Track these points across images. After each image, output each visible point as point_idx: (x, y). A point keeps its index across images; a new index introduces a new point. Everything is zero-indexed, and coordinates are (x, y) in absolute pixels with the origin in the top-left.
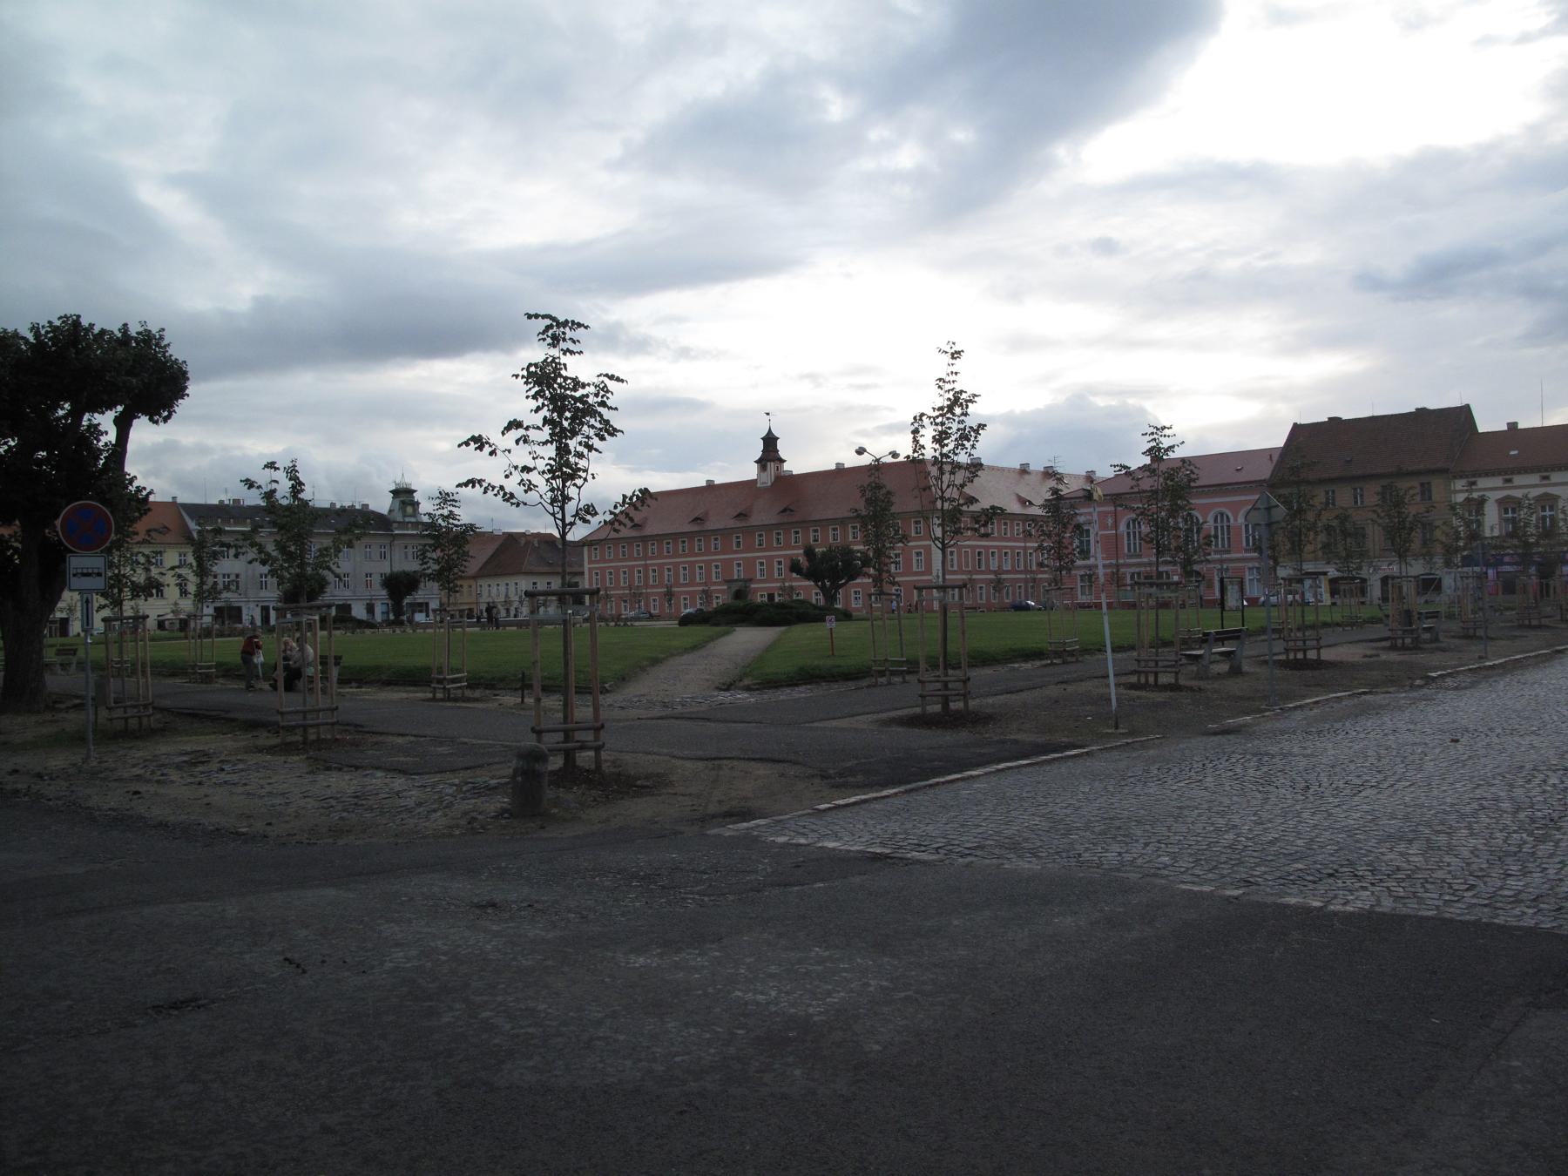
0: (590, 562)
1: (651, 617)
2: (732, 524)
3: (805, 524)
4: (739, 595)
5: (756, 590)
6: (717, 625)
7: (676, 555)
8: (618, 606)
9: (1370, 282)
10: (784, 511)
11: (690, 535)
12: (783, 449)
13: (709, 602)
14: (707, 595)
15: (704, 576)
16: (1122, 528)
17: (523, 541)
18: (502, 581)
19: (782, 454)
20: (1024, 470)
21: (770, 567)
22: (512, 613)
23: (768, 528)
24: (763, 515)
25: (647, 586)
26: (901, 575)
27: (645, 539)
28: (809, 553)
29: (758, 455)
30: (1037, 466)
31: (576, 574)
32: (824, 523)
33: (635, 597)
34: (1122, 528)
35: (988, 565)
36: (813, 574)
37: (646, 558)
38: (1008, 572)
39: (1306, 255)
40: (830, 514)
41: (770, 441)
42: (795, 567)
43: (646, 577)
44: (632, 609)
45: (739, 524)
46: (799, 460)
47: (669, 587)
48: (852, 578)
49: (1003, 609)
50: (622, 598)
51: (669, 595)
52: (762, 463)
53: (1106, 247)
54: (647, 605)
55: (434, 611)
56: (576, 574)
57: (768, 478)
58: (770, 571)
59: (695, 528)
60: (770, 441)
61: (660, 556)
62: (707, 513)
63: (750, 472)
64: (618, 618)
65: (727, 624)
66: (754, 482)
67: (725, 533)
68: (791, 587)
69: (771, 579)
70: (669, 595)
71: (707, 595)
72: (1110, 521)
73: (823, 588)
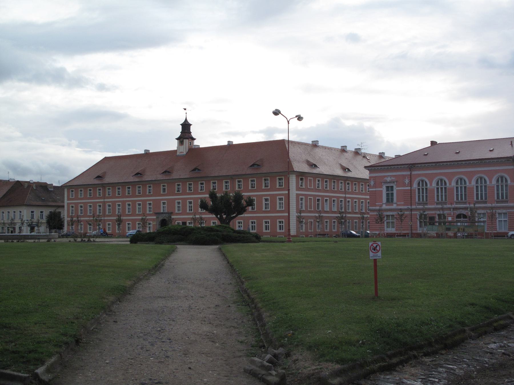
0: (69, 199)
1: (105, 235)
2: (160, 177)
3: (207, 178)
4: (164, 223)
5: (176, 219)
6: (161, 243)
7: (145, 195)
8: (86, 228)
9: (486, 63)
10: (194, 170)
11: (94, 186)
12: (194, 131)
13: (144, 226)
14: (144, 222)
15: (142, 210)
16: (415, 185)
17: (26, 185)
18: (11, 210)
19: (193, 135)
20: (343, 150)
21: (184, 206)
22: (17, 230)
23: (184, 180)
24: (181, 172)
25: (104, 215)
26: (83, 216)
27: (104, 186)
28: (213, 196)
29: (178, 134)
30: (351, 148)
31: (59, 207)
32: (220, 178)
33: (97, 221)
34: (415, 185)
35: (323, 207)
36: (214, 210)
37: (104, 197)
38: (350, 213)
39: (465, 47)
40: (224, 173)
41: (186, 126)
42: (204, 206)
43: (104, 210)
44: (94, 230)
45: (97, 182)
46: (204, 139)
47: (119, 216)
48: (240, 213)
49: (337, 236)
50: (88, 223)
51: (119, 221)
52: (181, 139)
53: (353, 38)
54: (104, 226)
55: (447, 233)
56: (59, 207)
57: (184, 150)
58: (187, 208)
59: (97, 182)
60: (186, 126)
61: (114, 197)
62: (105, 173)
63: (173, 145)
64: (85, 235)
65: (170, 242)
66: (175, 151)
67: (155, 183)
68: (201, 219)
69: (184, 213)
70: (119, 221)
71: (144, 222)
72: (407, 181)
73: (221, 219)
